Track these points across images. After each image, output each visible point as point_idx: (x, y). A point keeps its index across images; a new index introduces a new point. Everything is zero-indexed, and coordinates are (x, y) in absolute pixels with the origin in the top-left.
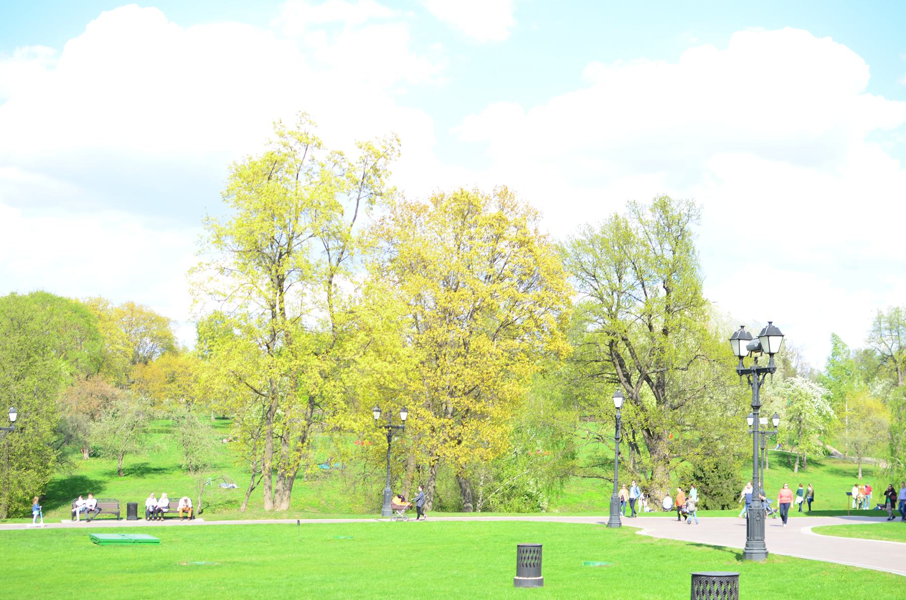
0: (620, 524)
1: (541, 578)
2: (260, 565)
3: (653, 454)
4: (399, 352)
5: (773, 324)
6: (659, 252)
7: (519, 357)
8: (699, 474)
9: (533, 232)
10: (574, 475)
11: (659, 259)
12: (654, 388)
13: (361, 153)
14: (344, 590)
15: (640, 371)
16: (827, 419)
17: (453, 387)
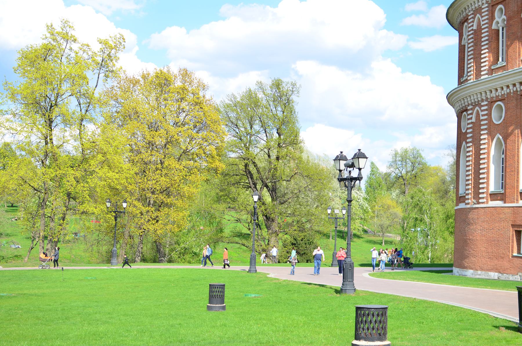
0: (256, 271)
1: (224, 305)
2: (41, 296)
3: (269, 230)
4: (123, 167)
5: (361, 151)
6: (275, 112)
7: (193, 171)
8: (294, 242)
9: (202, 97)
10: (222, 242)
11: (275, 116)
12: (270, 191)
13: (100, 46)
14: (100, 313)
15: (262, 182)
16: (365, 211)
17: (154, 189)
